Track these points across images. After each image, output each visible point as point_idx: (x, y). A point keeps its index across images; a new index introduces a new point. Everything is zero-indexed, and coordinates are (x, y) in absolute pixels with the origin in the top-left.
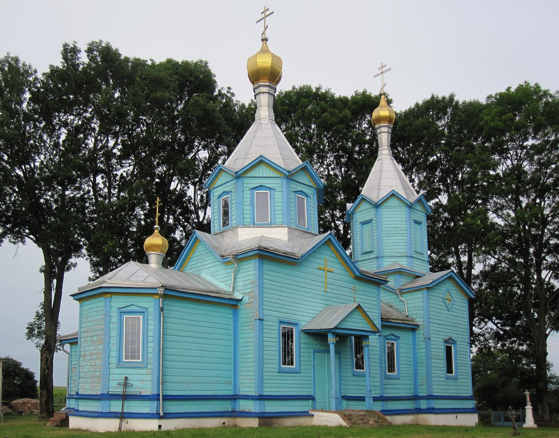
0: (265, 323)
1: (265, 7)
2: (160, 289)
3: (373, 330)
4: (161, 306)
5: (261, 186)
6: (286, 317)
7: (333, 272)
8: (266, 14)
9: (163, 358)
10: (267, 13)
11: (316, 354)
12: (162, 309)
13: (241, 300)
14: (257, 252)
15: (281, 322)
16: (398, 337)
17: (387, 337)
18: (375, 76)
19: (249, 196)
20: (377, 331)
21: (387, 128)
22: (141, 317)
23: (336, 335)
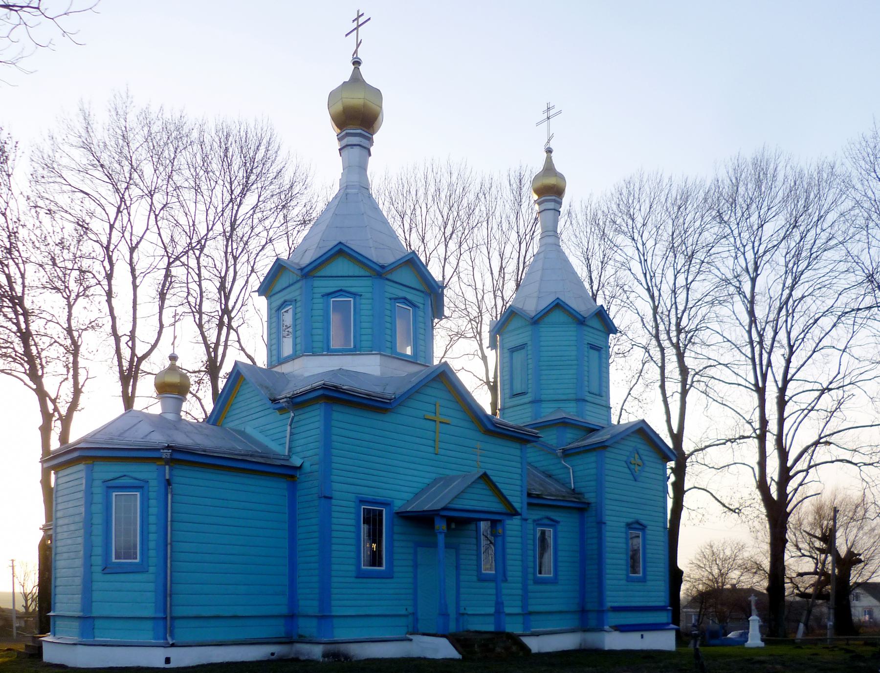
0: (334, 502)
1: (358, 11)
2: (165, 451)
3: (509, 511)
4: (167, 477)
5: (341, 290)
6: (368, 493)
7: (448, 424)
8: (359, 21)
9: (171, 557)
10: (361, 20)
11: (419, 549)
12: (168, 483)
13: (300, 467)
14: (321, 392)
15: (362, 501)
16: (557, 522)
17: (539, 522)
18: (538, 124)
19: (321, 306)
20: (514, 513)
21: (553, 203)
22: (138, 494)
23: (450, 520)
